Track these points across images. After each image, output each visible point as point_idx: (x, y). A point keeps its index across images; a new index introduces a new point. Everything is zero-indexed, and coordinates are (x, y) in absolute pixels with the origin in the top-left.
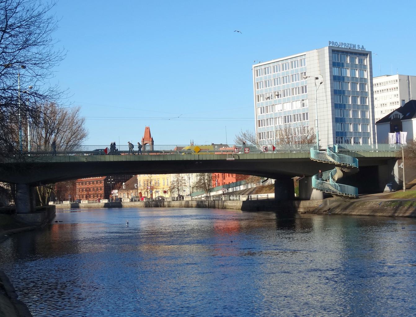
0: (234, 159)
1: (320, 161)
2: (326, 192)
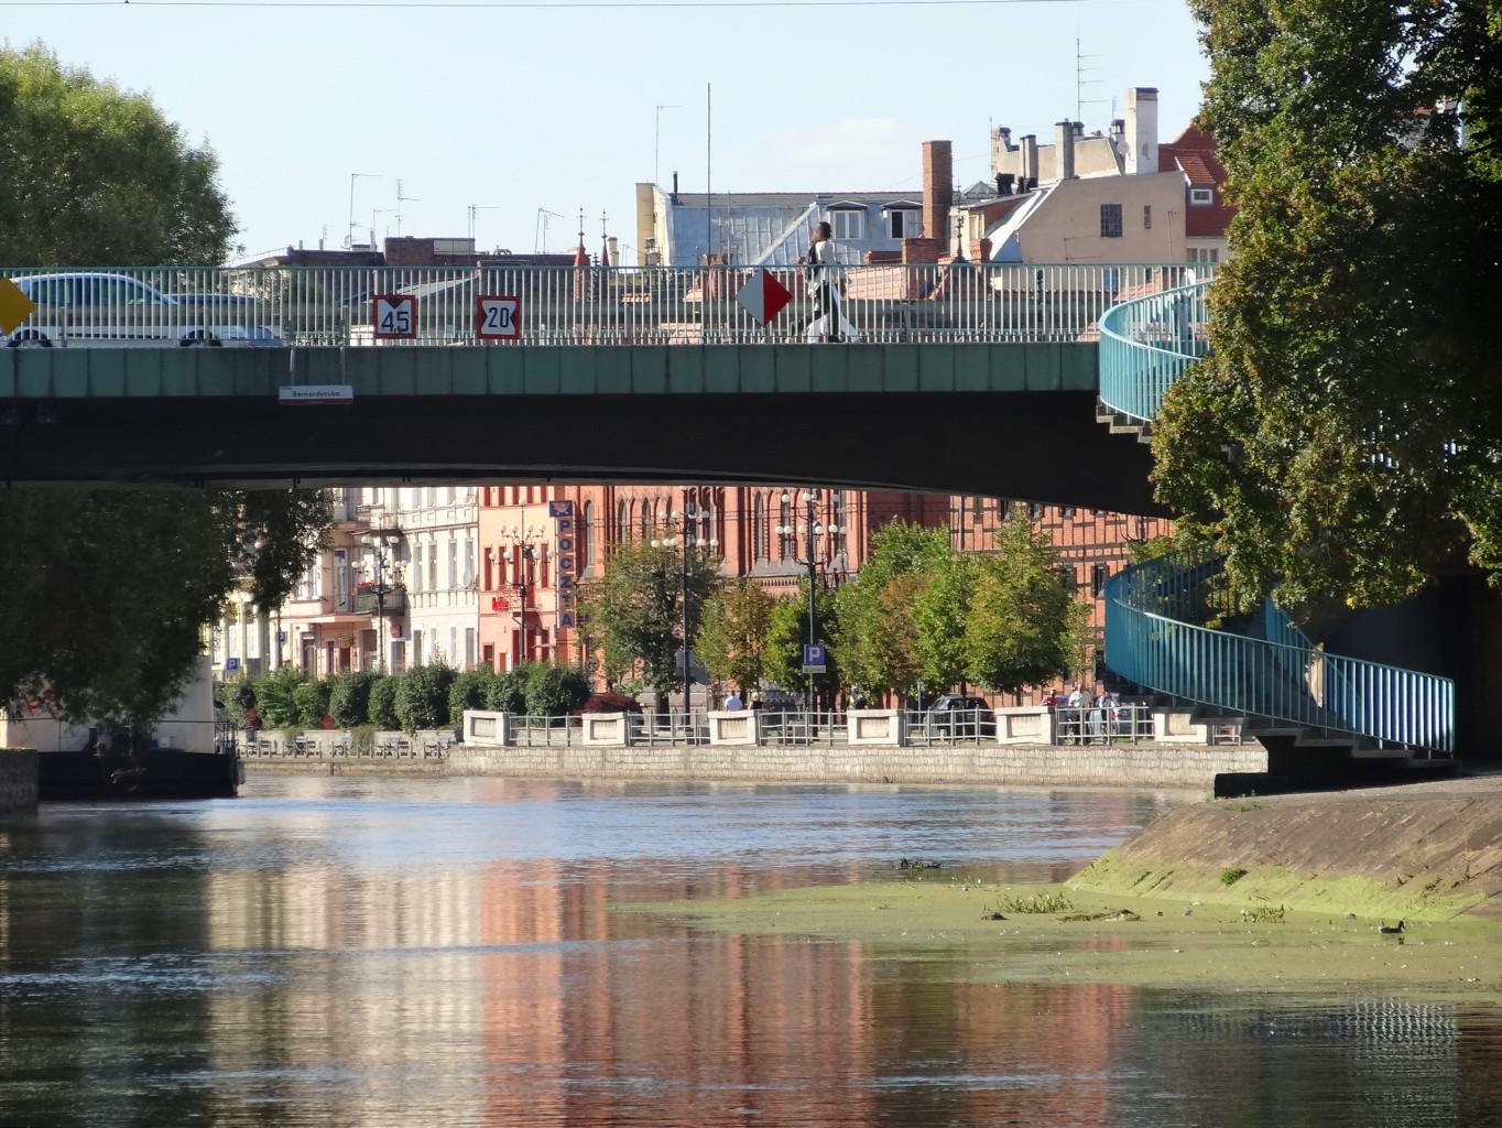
0: (346, 392)
1: (1122, 430)
2: (1113, 430)
